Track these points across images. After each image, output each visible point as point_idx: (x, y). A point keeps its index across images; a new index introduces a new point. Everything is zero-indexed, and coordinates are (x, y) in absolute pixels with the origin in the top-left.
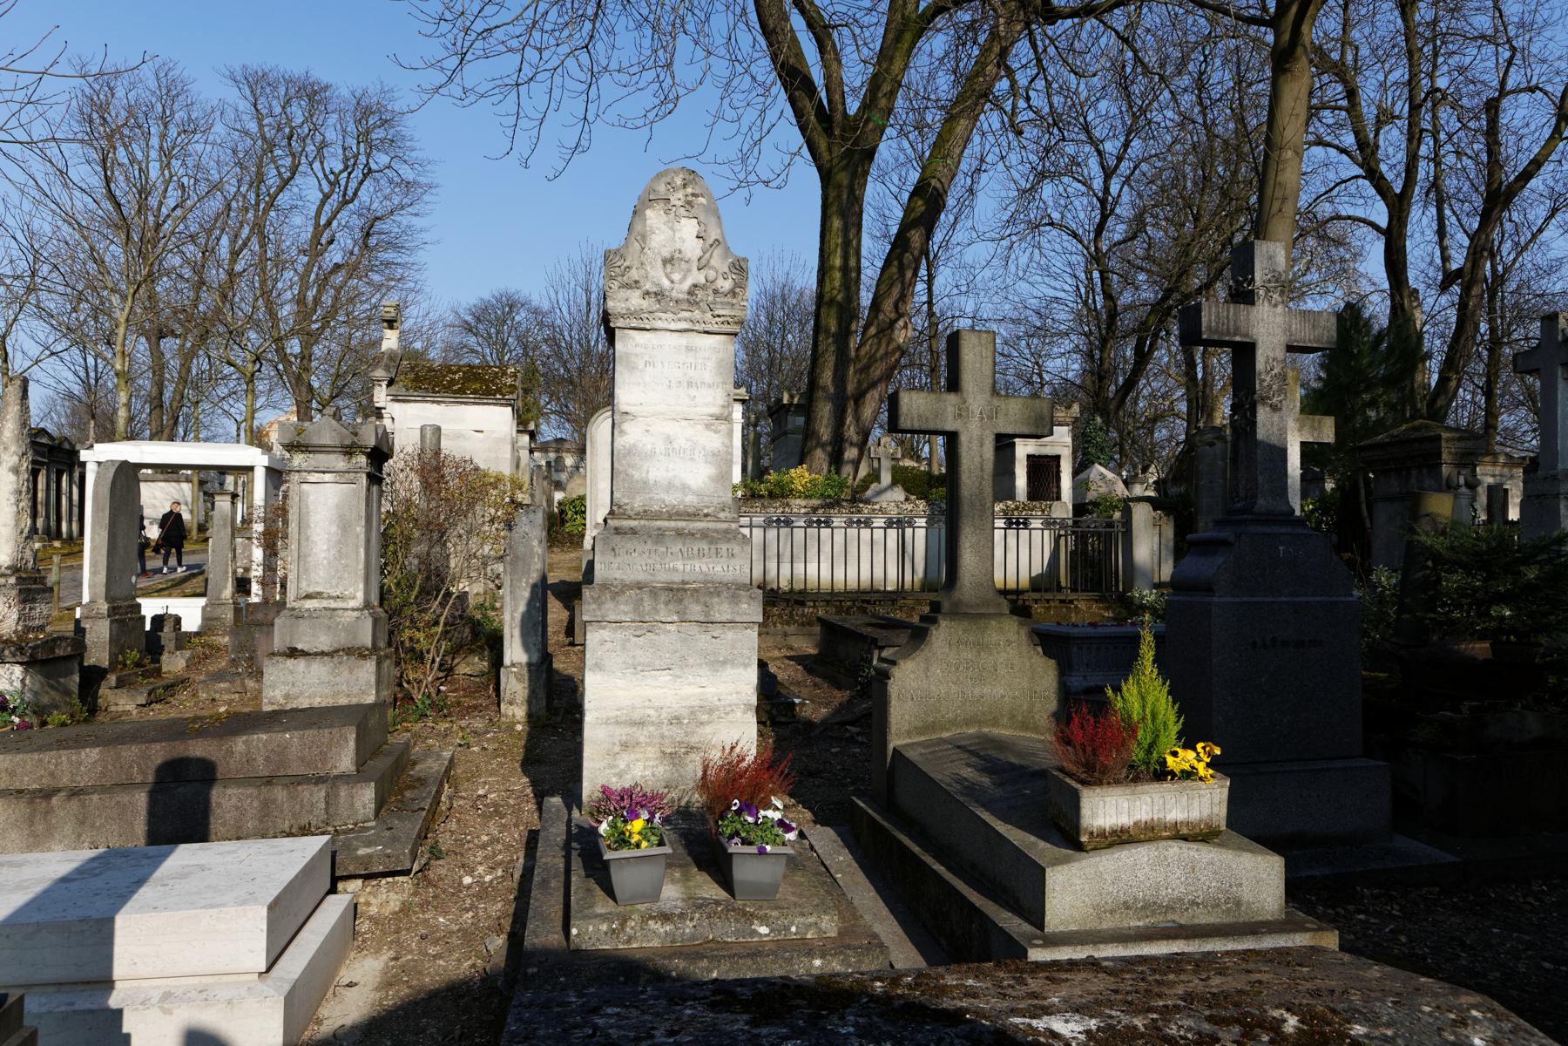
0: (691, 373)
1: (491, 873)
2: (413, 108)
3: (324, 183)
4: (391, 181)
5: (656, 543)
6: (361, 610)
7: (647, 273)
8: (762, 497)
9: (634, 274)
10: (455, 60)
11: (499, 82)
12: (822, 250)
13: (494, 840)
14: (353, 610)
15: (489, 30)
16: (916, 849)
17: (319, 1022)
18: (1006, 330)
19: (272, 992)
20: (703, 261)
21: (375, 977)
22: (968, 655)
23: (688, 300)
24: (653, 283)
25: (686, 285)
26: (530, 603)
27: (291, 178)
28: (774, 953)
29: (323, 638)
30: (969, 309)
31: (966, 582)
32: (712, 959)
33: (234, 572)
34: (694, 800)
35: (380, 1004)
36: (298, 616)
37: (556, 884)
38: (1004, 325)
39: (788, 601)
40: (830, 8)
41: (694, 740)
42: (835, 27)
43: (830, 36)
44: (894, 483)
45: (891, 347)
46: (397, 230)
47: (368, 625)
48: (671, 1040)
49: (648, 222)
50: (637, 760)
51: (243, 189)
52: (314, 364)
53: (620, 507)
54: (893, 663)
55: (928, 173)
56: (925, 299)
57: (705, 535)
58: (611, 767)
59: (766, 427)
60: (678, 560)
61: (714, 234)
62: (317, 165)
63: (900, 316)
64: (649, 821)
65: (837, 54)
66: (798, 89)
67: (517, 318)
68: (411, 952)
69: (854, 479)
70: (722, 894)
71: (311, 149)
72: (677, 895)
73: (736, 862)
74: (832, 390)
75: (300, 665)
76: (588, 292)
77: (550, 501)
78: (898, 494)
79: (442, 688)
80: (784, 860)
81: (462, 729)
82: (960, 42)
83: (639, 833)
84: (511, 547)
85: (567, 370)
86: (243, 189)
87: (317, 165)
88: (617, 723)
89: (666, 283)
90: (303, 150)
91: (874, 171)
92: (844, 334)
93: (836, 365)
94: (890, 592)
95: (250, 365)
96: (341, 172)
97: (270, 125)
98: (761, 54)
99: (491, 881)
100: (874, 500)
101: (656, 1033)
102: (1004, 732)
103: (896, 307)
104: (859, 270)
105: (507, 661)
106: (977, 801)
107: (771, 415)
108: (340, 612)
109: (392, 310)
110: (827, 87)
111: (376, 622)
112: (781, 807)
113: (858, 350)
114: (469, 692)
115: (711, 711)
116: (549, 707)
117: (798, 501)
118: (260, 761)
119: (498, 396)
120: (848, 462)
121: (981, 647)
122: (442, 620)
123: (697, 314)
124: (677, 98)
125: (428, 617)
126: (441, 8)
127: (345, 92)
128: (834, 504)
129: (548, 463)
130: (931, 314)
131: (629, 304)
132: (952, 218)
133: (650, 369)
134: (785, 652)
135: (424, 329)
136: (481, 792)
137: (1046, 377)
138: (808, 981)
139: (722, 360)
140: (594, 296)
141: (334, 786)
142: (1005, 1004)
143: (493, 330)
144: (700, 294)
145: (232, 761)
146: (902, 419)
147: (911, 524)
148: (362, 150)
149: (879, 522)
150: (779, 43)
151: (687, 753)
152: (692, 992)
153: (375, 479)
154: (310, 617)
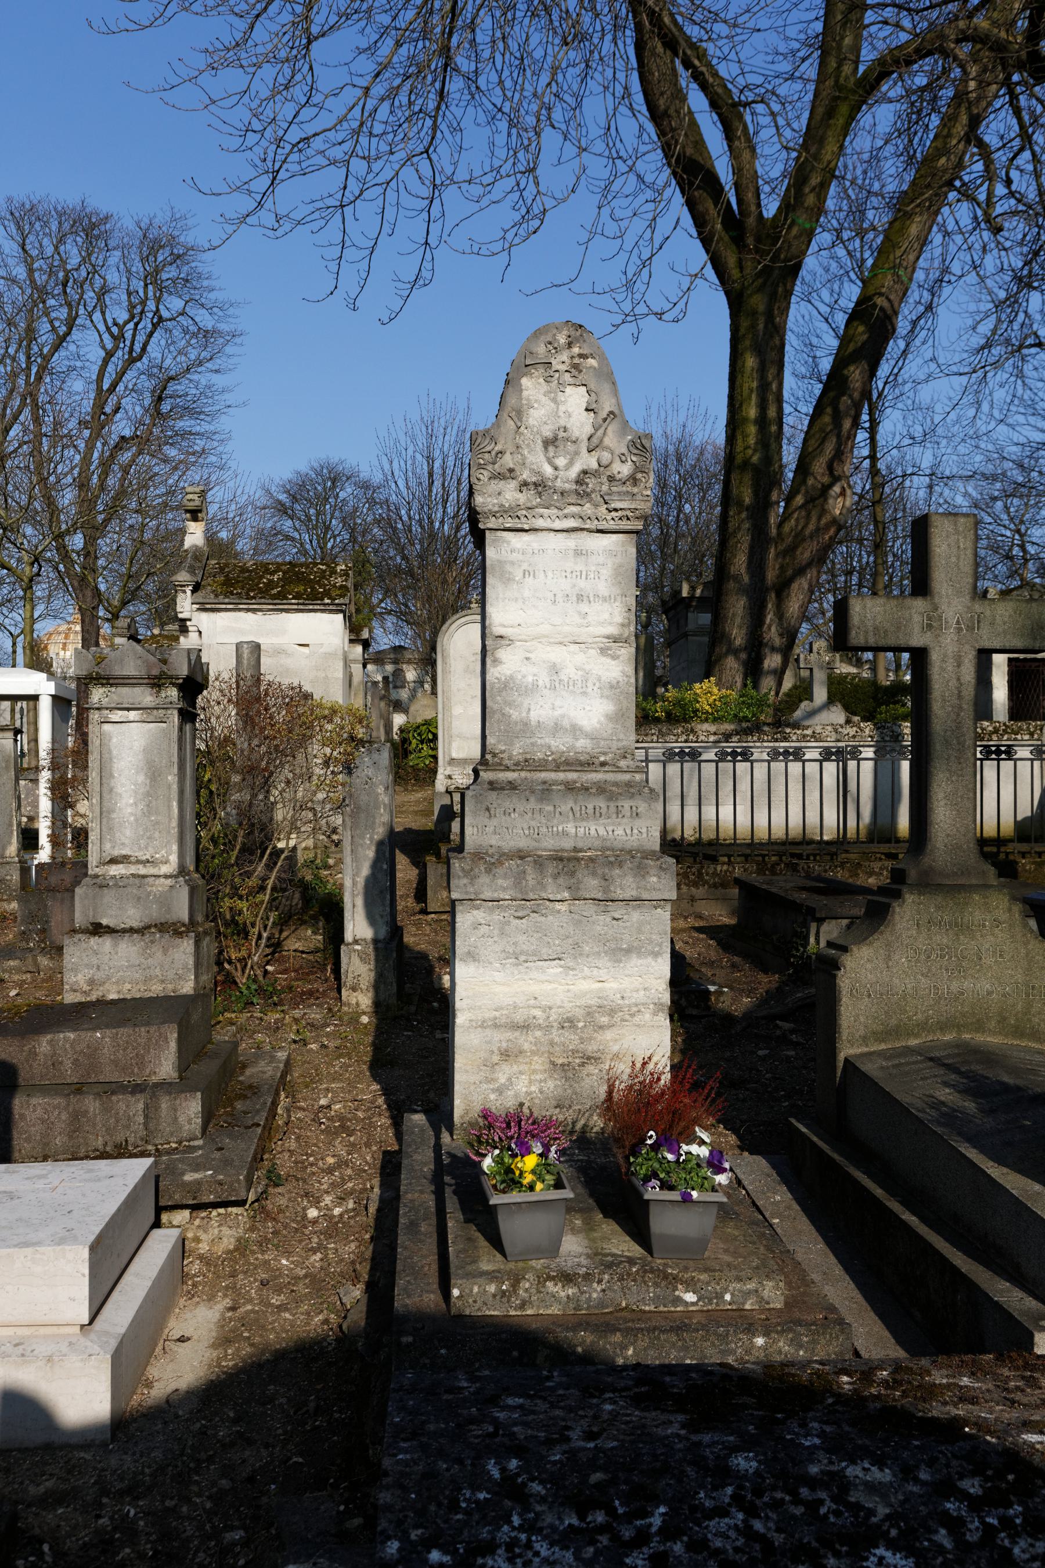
0: (582, 583)
1: (339, 1205)
2: (215, 244)
3: (106, 337)
4: (186, 331)
6: (176, 877)
7: (524, 458)
8: (657, 720)
9: (508, 461)
10: (266, 180)
12: (731, 397)
13: (342, 1164)
14: (166, 877)
15: (306, 139)
16: (879, 1192)
17: (149, 1385)
18: (975, 488)
19: (96, 1349)
20: (595, 441)
21: (211, 1330)
22: (943, 939)
25: (574, 472)
26: (375, 865)
27: (68, 333)
28: (704, 1327)
29: (131, 912)
30: (926, 463)
31: (940, 845)
32: (627, 1332)
33: (19, 824)
34: (591, 1123)
35: (219, 1366)
36: (102, 884)
37: (428, 1227)
38: (972, 483)
39: (695, 855)
40: (740, 79)
41: (591, 1048)
42: (747, 104)
43: (741, 117)
44: (831, 701)
45: (824, 521)
47: (184, 894)
48: (591, 1445)
49: (525, 394)
50: (521, 1073)
51: (11, 351)
52: (101, 562)
53: (495, 755)
54: (844, 949)
55: (871, 290)
56: (866, 452)
57: (601, 789)
58: (489, 1081)
59: (661, 624)
60: (568, 822)
61: (607, 405)
62: (97, 316)
63: (836, 479)
64: (543, 1155)
65: (749, 140)
66: (698, 188)
68: (250, 1301)
69: (777, 694)
70: (635, 1250)
71: (90, 295)
72: (580, 1250)
73: (653, 1210)
74: (746, 579)
75: (106, 943)
76: (430, 459)
77: (388, 726)
78: (837, 715)
79: (269, 968)
80: (714, 1210)
81: (296, 1020)
82: (915, 116)
83: (533, 1172)
84: (351, 796)
85: (404, 558)
86: (11, 351)
87: (97, 316)
88: (496, 1026)
89: (548, 470)
90: (81, 298)
91: (798, 288)
92: (762, 506)
93: (752, 548)
94: (828, 843)
95: (27, 569)
96: (126, 323)
97: (41, 269)
98: (650, 147)
99: (341, 1215)
100: (806, 723)
101: (571, 1434)
102: (992, 1040)
103: (830, 468)
105: (348, 937)
106: (960, 1134)
107: (665, 612)
108: (151, 880)
110: (737, 185)
111: (193, 891)
112: (708, 1140)
113: (780, 525)
114: (303, 974)
115: (612, 1012)
116: (400, 993)
117: (706, 726)
118: (68, 1064)
119: (327, 601)
120: (769, 672)
121: (961, 928)
122: (270, 883)
123: (588, 509)
125: (253, 882)
126: (247, 116)
127: (129, 224)
128: (750, 728)
129: (385, 679)
130: (874, 471)
132: (902, 344)
133: (529, 580)
134: (692, 922)
135: (231, 515)
136: (323, 1102)
137: (1032, 549)
138: (754, 1371)
139: (620, 566)
140: (437, 464)
141: (153, 1096)
142: (1013, 1415)
143: (312, 511)
144: (592, 483)
145: (35, 1065)
146: (853, 633)
147: (855, 754)
148: (150, 294)
149: (812, 754)
150: (673, 130)
151: (583, 1064)
152: (609, 1379)
153: (188, 716)
154: (116, 885)
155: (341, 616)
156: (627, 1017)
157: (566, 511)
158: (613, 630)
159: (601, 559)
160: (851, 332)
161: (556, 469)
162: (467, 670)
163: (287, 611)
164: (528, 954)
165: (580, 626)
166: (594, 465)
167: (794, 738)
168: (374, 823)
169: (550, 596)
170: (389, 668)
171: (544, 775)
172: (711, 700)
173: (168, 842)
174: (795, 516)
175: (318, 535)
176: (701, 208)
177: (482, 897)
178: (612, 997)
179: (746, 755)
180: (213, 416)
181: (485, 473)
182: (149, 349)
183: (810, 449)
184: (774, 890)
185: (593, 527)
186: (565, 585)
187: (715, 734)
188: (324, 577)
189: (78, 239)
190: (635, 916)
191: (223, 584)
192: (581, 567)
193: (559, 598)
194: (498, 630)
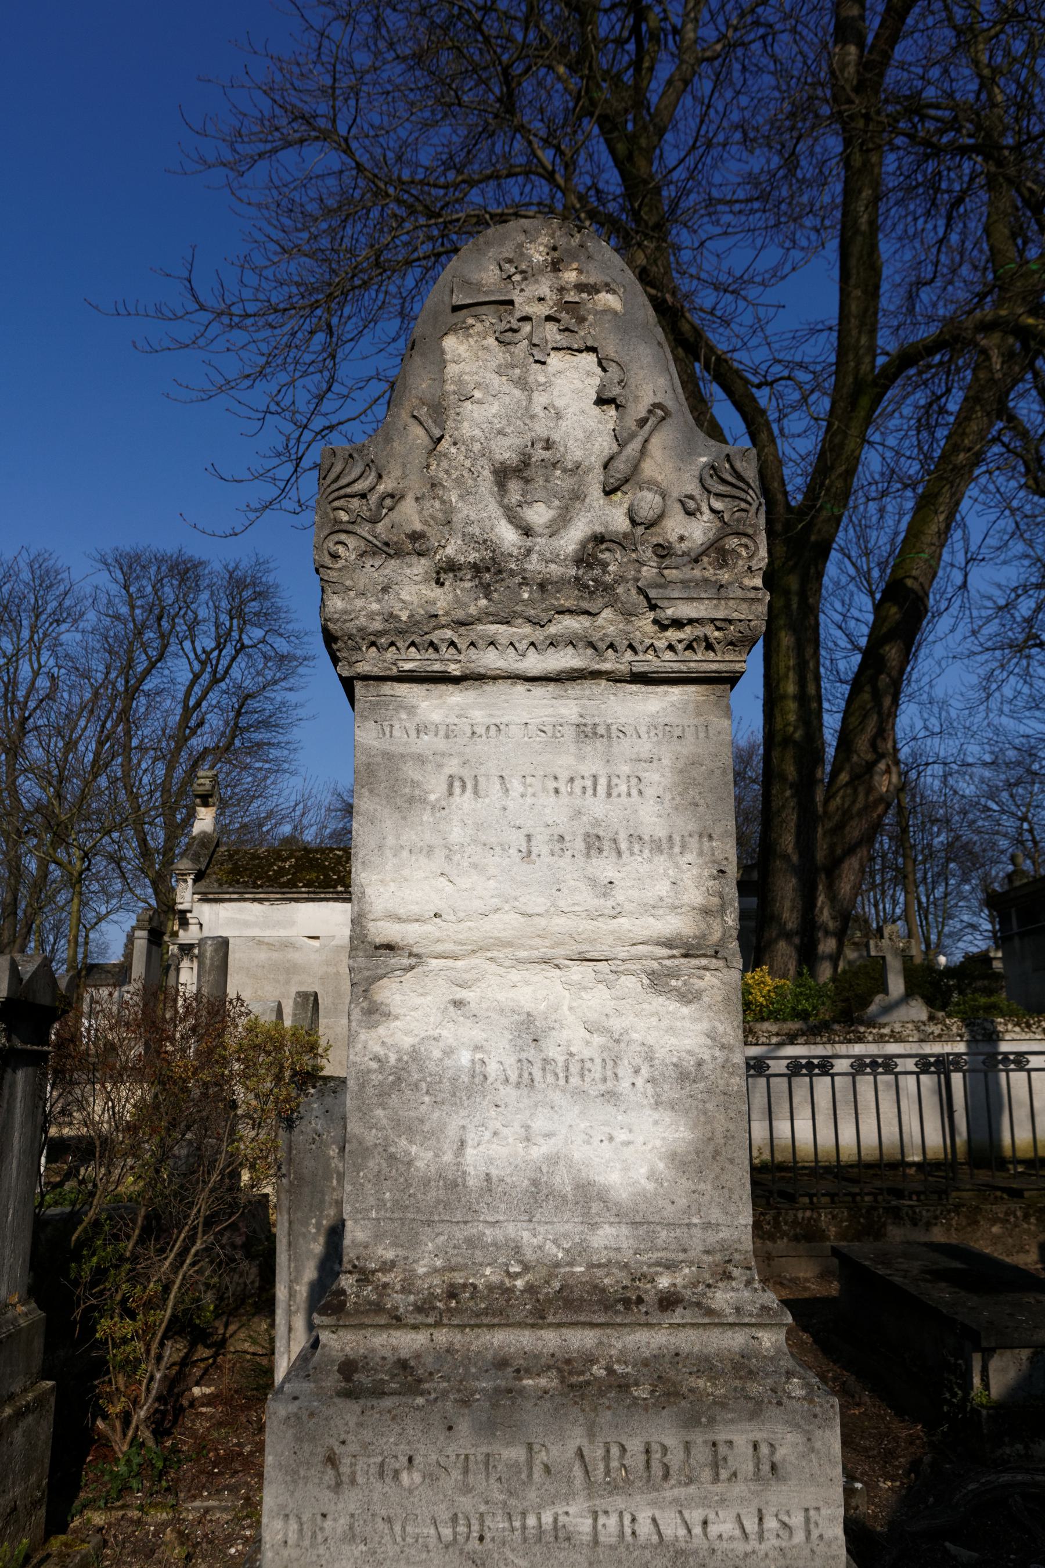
0: (597, 807)
5: (489, 1428)
7: (449, 510)
10: (289, 467)
12: (767, 676)
15: (331, 428)
45: (871, 798)
49: (452, 369)
53: (365, 1277)
60: (569, 1496)
62: (187, 644)
63: (881, 756)
71: (182, 628)
74: (795, 858)
78: (918, 1011)
86: (113, 675)
87: (187, 644)
89: (508, 536)
90: (173, 627)
92: (805, 785)
93: (798, 826)
95: (78, 863)
100: (883, 1020)
103: (873, 745)
113: (826, 802)
117: (766, 1025)
119: (340, 889)
127: (217, 566)
131: (391, 603)
133: (463, 801)
139: (694, 762)
144: (615, 562)
157: (552, 629)
159: (645, 747)
161: (527, 532)
163: (296, 900)
165: (594, 916)
166: (620, 523)
167: (870, 1038)
168: (322, 1201)
169: (517, 839)
171: (501, 1339)
172: (765, 992)
174: (841, 793)
179: (824, 1067)
181: (351, 542)
184: (897, 1279)
185: (623, 668)
187: (777, 1034)
188: (340, 863)
191: (229, 873)
193: (539, 843)
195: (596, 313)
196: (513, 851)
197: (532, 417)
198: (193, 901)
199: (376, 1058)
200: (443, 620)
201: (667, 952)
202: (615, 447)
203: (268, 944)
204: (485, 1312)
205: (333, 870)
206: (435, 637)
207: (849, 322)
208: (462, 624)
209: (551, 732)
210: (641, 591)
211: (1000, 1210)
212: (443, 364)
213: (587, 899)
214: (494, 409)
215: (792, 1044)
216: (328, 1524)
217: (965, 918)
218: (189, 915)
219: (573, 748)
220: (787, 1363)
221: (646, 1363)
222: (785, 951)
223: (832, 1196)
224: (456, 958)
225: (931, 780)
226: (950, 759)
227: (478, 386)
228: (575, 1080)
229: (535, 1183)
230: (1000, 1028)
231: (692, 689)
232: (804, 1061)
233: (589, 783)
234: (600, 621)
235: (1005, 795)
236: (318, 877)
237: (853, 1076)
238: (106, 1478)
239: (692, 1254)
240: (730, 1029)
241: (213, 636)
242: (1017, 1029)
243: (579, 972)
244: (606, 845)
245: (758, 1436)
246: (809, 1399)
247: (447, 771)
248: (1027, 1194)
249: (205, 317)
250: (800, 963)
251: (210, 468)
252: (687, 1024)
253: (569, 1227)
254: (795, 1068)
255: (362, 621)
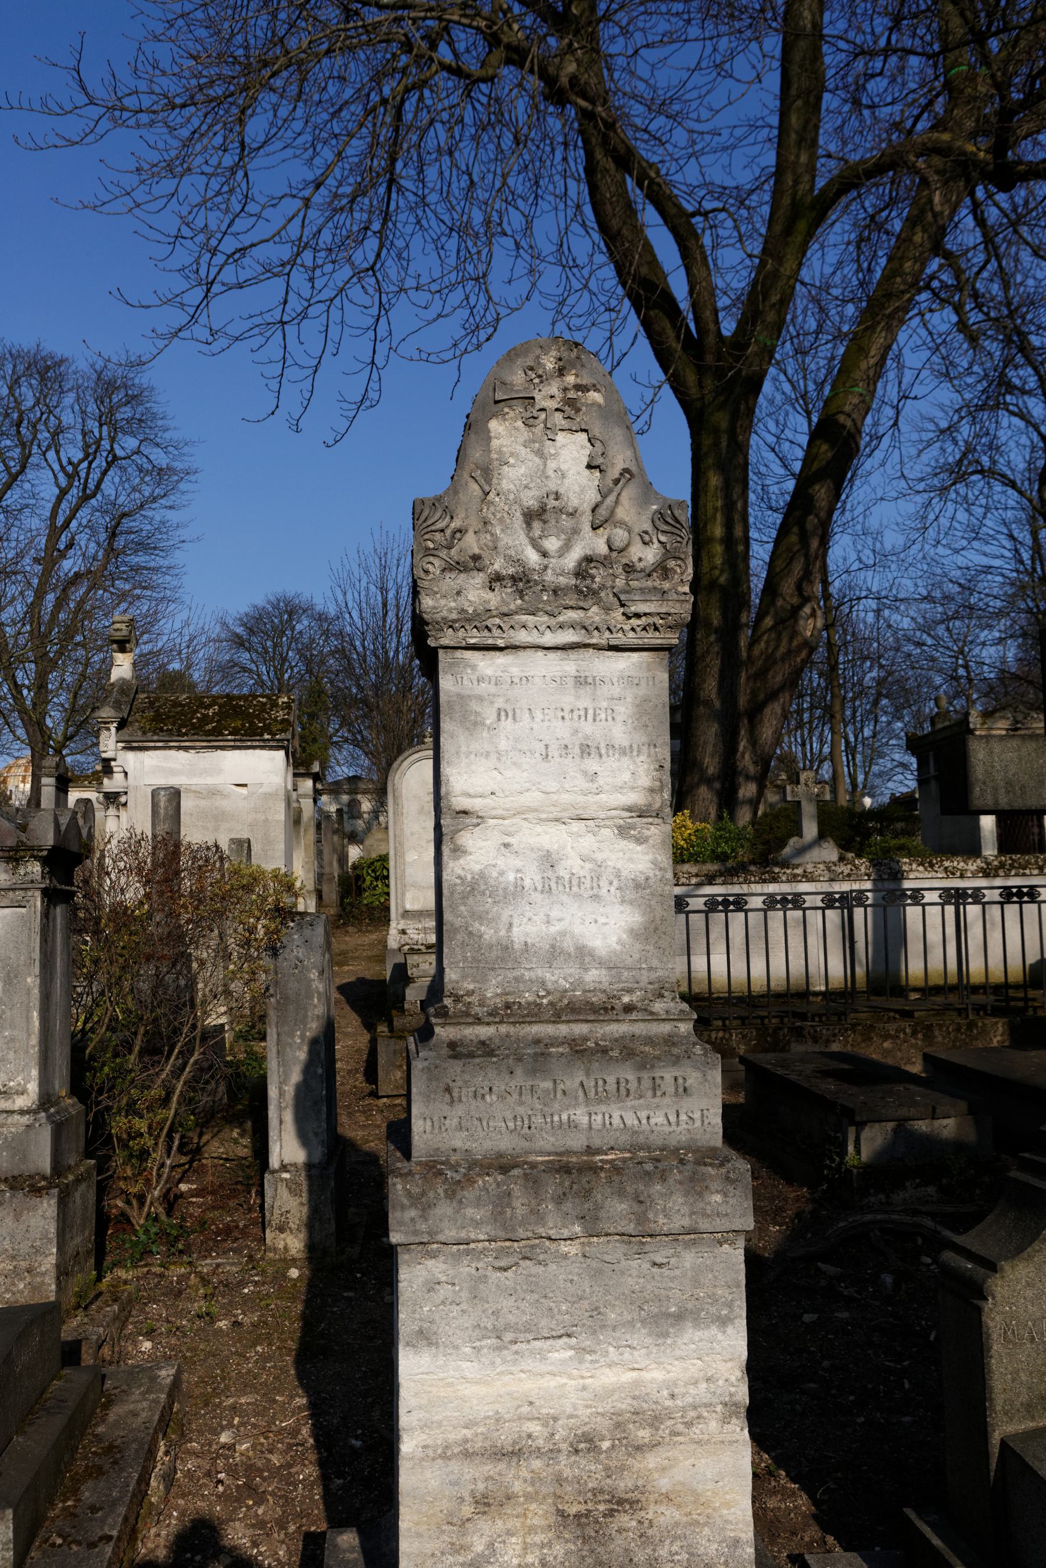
0: (587, 728)
5: (532, 1072)
7: (495, 539)
9: (471, 543)
10: (199, 293)
11: (258, 320)
14: (22, 1112)
15: (243, 251)
20: (603, 512)
23: (577, 589)
24: (508, 558)
27: (22, 471)
41: (623, 1484)
44: (822, 836)
45: (795, 643)
46: (149, 527)
47: (45, 1137)
49: (495, 443)
50: (510, 1533)
53: (457, 999)
60: (576, 1106)
61: (620, 459)
62: (51, 455)
63: (806, 600)
67: (299, 627)
71: (44, 435)
74: (717, 704)
76: (384, 590)
77: (343, 858)
78: (829, 852)
84: (277, 983)
85: (360, 688)
87: (51, 455)
88: (467, 1455)
89: (532, 557)
90: (35, 437)
92: (730, 631)
93: (722, 671)
100: (796, 861)
103: (799, 588)
104: (747, 540)
105: (274, 1162)
109: (123, 626)
110: (694, 306)
115: (655, 1421)
119: (267, 737)
120: (744, 802)
123: (595, 614)
124: (498, 320)
125: (156, 1092)
127: (82, 365)
129: (339, 811)
133: (507, 724)
139: (646, 700)
140: (391, 595)
143: (269, 643)
144: (599, 575)
148: (105, 433)
151: (610, 1513)
155: (281, 753)
156: (680, 1428)
157: (561, 618)
158: (635, 798)
160: (815, 450)
161: (545, 554)
162: (421, 811)
163: (223, 748)
164: (517, 1330)
166: (602, 549)
167: (784, 878)
168: (305, 1016)
169: (540, 747)
170: (345, 798)
171: (536, 1030)
172: (686, 835)
173: (27, 1065)
174: (765, 638)
175: (275, 667)
176: (657, 327)
177: (441, 1238)
178: (655, 1396)
179: (739, 904)
180: (166, 551)
181: (437, 562)
182: (103, 486)
183: (778, 570)
184: (793, 1077)
185: (603, 642)
186: (562, 730)
187: (697, 875)
188: (264, 711)
189: (33, 382)
190: (689, 1259)
191: (152, 720)
192: (584, 702)
193: (554, 752)
194: (459, 802)
195: (587, 405)
196: (537, 755)
197: (547, 477)
198: (116, 750)
199: (459, 877)
200: (494, 613)
201: (629, 814)
202: (599, 497)
203: (195, 792)
204: (527, 1015)
205: (257, 717)
206: (489, 623)
207: (789, 136)
208: (506, 615)
209: (559, 681)
210: (615, 595)
211: (892, 1028)
212: (489, 439)
213: (582, 783)
214: (522, 470)
215: (711, 884)
216: (447, 1122)
217: (897, 757)
218: (113, 763)
219: (572, 691)
220: (694, 1038)
221: (616, 1040)
222: (706, 798)
223: (743, 1019)
224: (504, 819)
225: (864, 614)
226: (883, 593)
227: (512, 454)
228: (575, 889)
229: (553, 946)
230: (905, 868)
231: (645, 654)
232: (720, 899)
233: (582, 713)
234: (590, 613)
235: (941, 630)
236: (243, 725)
237: (765, 911)
238: (127, 1245)
239: (642, 984)
240: (665, 859)
241: (81, 444)
242: (921, 868)
243: (576, 826)
244: (593, 750)
245: (677, 1074)
246: (705, 1055)
247: (496, 706)
248: (916, 1014)
249: (95, 112)
250: (720, 809)
251: (116, 293)
252: (640, 856)
253: (572, 970)
254: (712, 905)
255: (445, 613)
